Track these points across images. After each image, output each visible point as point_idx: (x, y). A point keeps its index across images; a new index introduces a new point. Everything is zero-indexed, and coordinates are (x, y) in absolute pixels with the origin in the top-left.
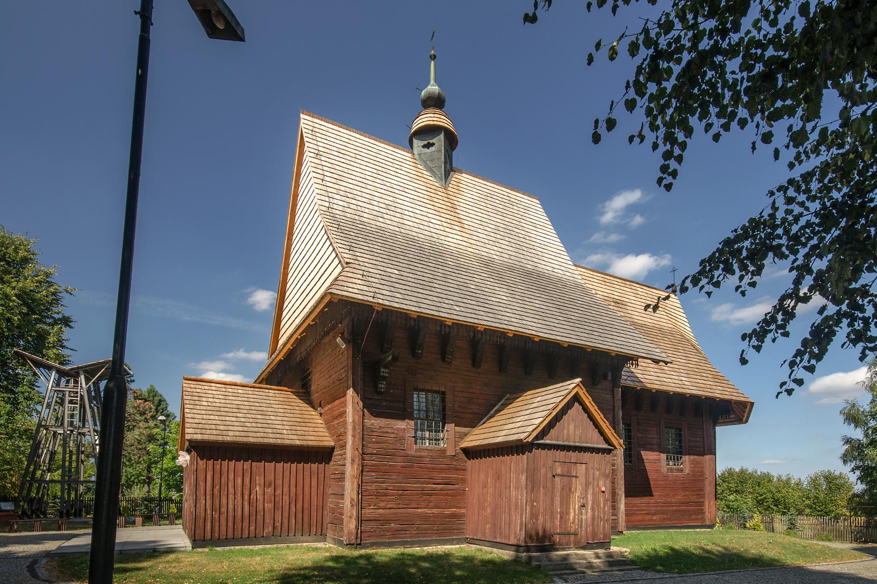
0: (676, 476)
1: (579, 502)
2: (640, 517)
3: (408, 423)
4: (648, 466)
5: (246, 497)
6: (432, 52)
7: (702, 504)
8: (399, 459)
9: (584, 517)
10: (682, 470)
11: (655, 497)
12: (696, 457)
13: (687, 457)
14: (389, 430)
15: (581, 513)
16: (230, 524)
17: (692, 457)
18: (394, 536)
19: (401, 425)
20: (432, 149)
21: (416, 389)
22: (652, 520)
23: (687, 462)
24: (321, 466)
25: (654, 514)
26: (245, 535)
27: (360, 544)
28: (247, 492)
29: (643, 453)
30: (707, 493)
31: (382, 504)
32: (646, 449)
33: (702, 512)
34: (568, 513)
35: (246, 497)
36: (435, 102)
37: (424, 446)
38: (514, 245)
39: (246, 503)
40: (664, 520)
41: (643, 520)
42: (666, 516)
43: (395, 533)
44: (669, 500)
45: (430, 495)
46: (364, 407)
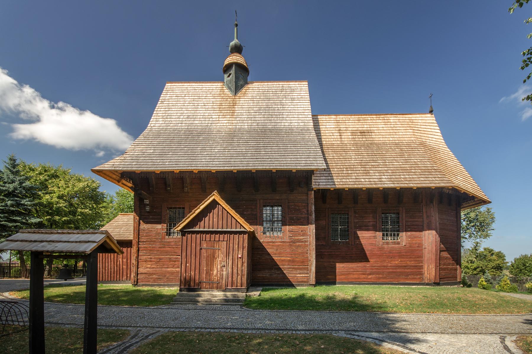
0: (392, 247)
1: (221, 264)
2: (356, 276)
3: (162, 226)
4: (363, 242)
5: (115, 263)
6: (236, 23)
7: (421, 267)
8: (158, 244)
9: (224, 273)
10: (398, 243)
11: (371, 263)
12: (414, 233)
13: (404, 233)
14: (153, 230)
15: (222, 271)
16: (109, 275)
17: (409, 233)
18: (154, 281)
19: (159, 226)
20: (231, 76)
21: (265, 206)
22: (367, 278)
23: (404, 238)
24: (129, 249)
25: (370, 274)
26: (107, 280)
27: (137, 285)
28: (115, 261)
29: (358, 232)
30: (426, 259)
31: (149, 266)
32: (361, 229)
33: (421, 274)
34: (212, 270)
35: (115, 263)
36: (237, 49)
37: (174, 237)
38: (294, 114)
39: (115, 266)
40: (379, 278)
41: (359, 278)
42: (381, 276)
43: (155, 280)
44: (385, 264)
45: (175, 261)
46: (140, 219)
